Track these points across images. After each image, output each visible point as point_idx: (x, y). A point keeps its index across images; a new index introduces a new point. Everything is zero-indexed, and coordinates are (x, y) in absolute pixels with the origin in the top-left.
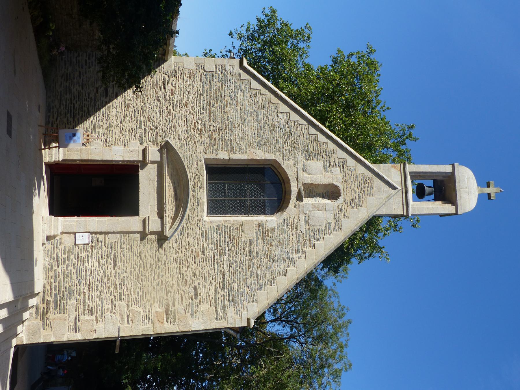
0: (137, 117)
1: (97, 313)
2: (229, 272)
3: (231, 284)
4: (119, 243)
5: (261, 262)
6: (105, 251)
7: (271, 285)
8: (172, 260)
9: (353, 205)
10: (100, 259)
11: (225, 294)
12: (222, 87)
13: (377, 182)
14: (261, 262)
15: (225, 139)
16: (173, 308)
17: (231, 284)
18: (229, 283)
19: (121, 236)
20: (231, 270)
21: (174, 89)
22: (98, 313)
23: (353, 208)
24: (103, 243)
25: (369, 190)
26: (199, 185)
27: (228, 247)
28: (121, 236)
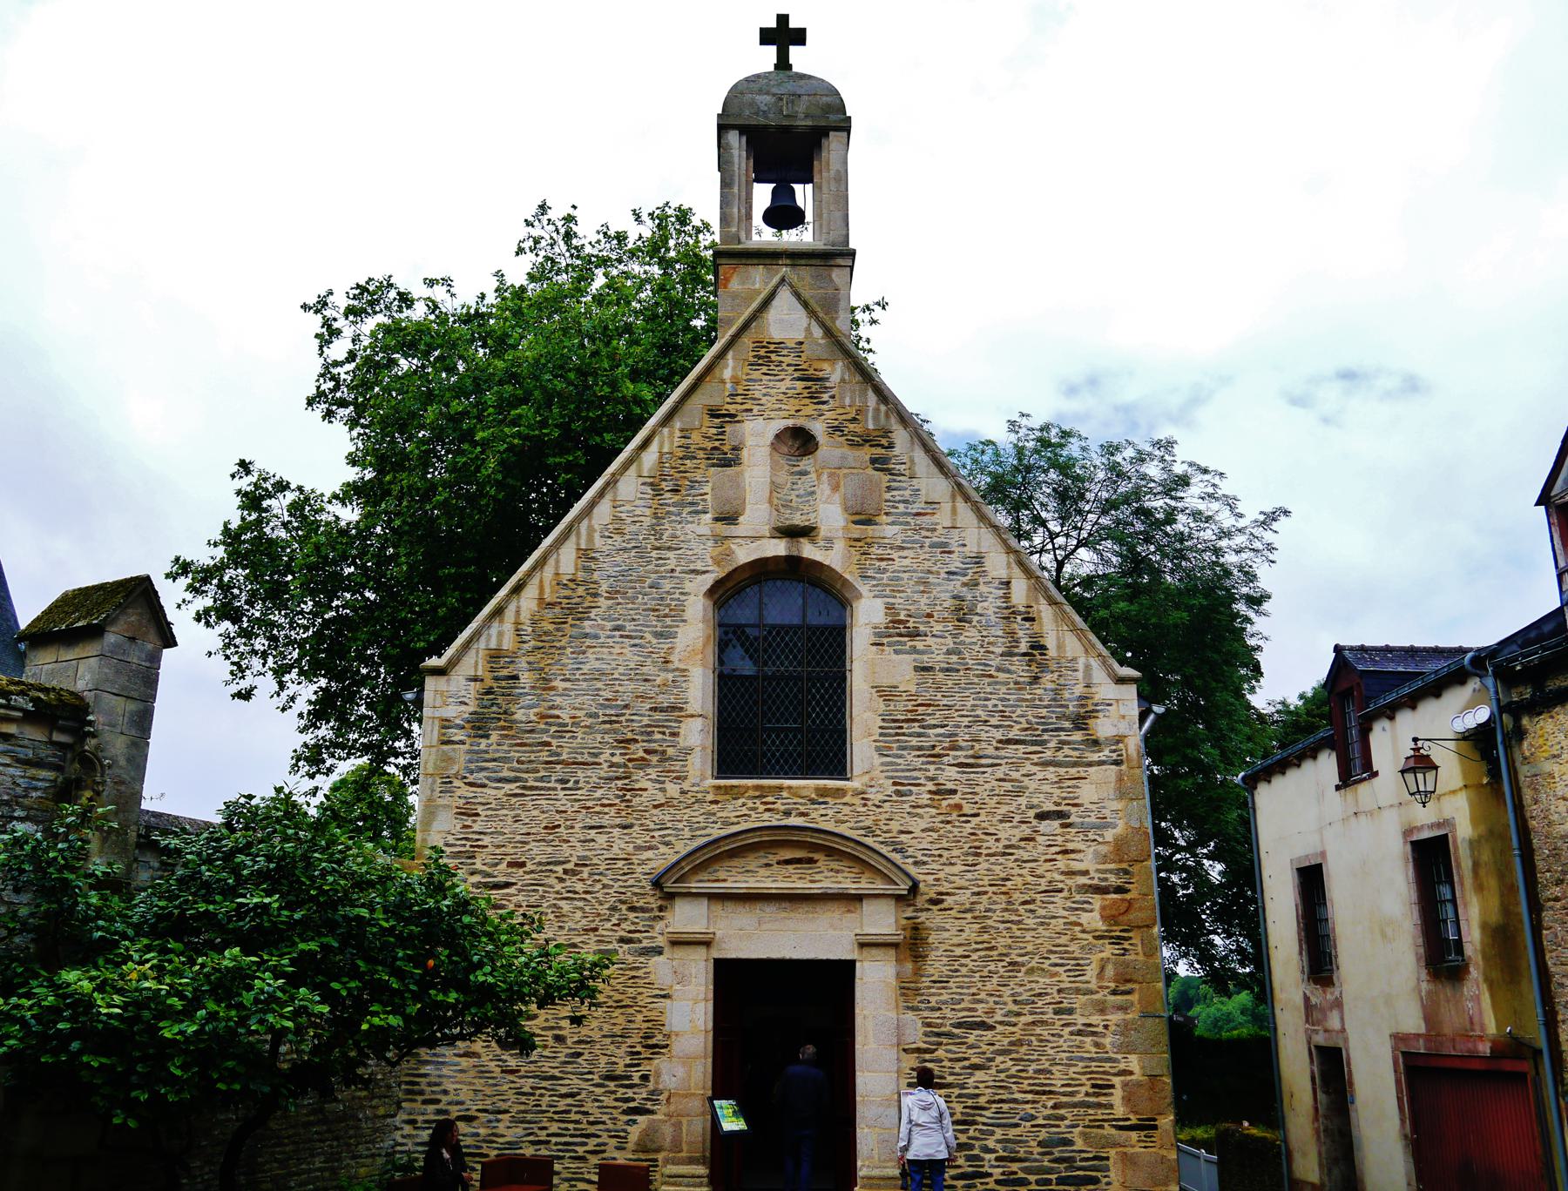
3: (1028, 722)
4: (926, 1014)
17: (1028, 722)
20: (994, 721)
21: (508, 859)
27: (935, 726)
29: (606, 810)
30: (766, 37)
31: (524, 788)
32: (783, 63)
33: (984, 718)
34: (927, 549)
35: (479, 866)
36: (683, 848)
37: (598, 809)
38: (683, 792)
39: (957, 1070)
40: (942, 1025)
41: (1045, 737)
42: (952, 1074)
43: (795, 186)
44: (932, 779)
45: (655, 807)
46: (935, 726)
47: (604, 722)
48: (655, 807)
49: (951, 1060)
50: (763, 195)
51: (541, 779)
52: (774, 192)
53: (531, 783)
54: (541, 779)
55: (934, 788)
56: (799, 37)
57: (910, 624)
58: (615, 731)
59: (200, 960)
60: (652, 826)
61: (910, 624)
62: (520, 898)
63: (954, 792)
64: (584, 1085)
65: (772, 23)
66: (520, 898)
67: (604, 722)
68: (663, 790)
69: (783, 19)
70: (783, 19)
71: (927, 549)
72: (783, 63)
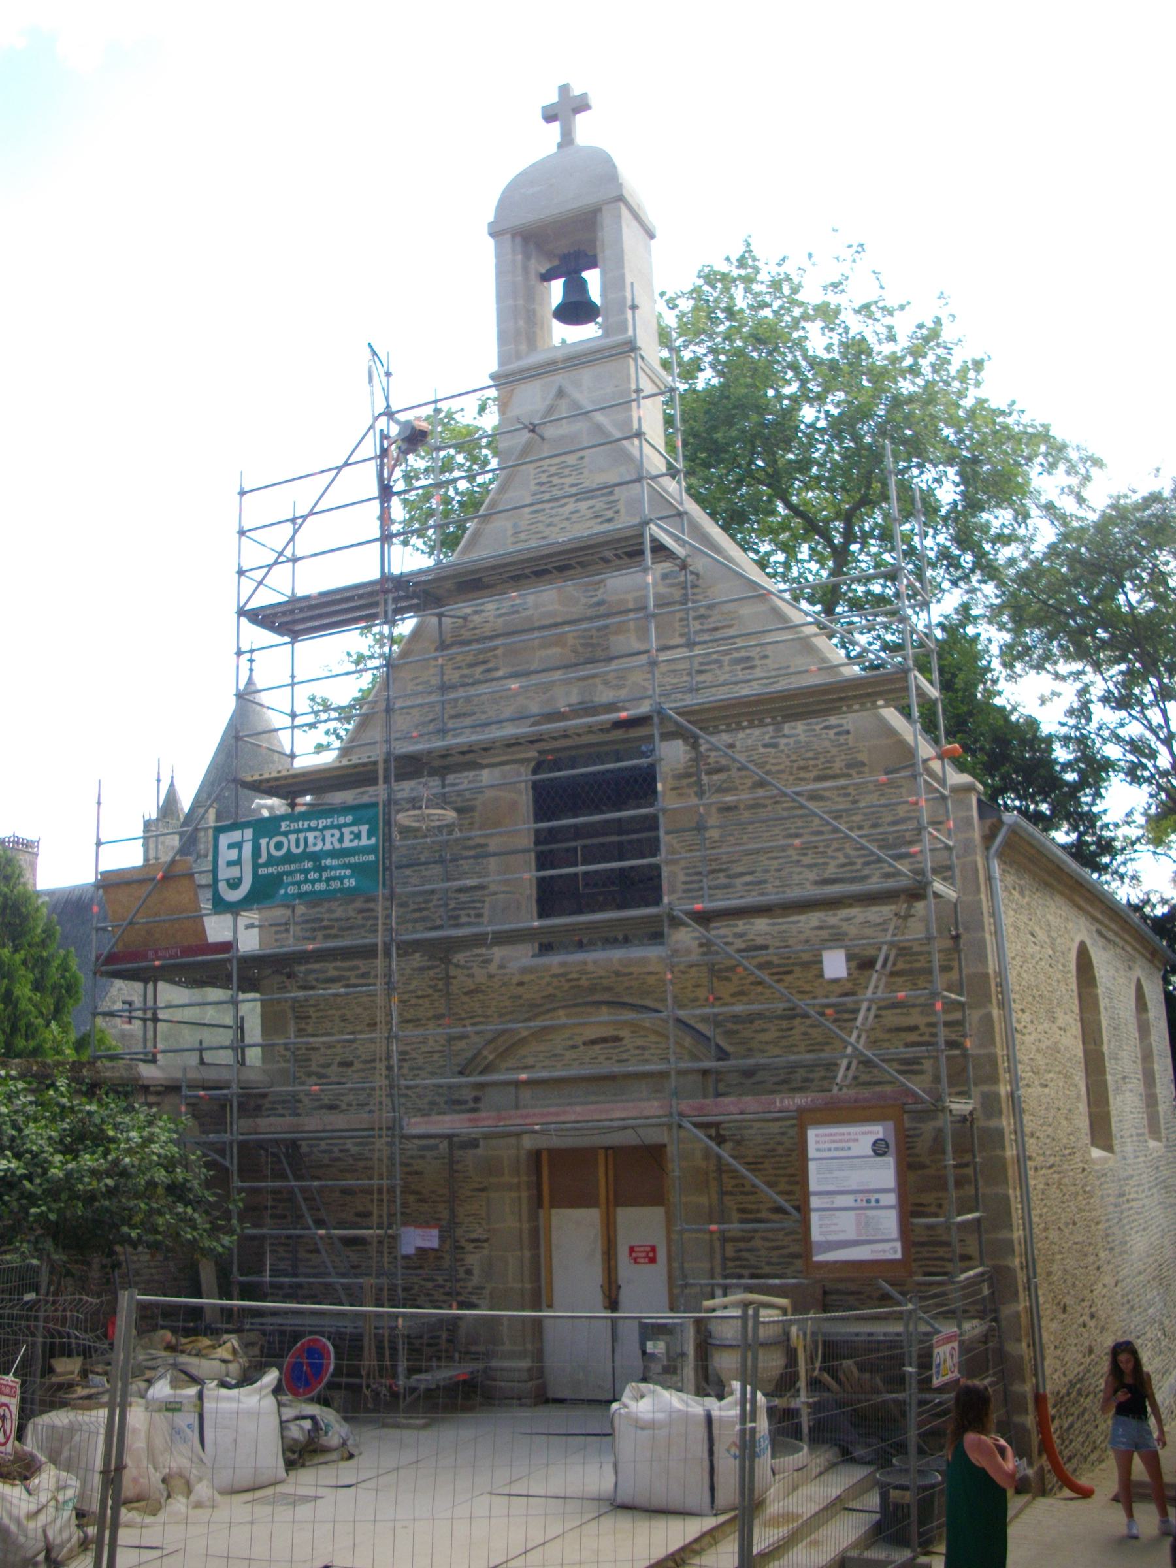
0: (412, 1157)
1: (942, 1259)
2: (815, 865)
3: (847, 856)
4: (740, 1198)
5: (782, 771)
6: (765, 1239)
7: (848, 732)
8: (784, 1043)
9: (610, 514)
10: (785, 1252)
11: (877, 873)
12: (326, 928)
13: (618, 1372)
14: (782, 771)
15: (455, 909)
16: (923, 1029)
17: (847, 856)
18: (843, 865)
19: (528, 851)
20: (807, 860)
21: (338, 1059)
22: (941, 1254)
23: (617, 512)
24: (742, 1245)
25: (567, 472)
26: (574, 976)
27: (742, 874)
28: (528, 851)
29: (421, 1001)
30: (550, 116)
31: (347, 986)
32: (567, 138)
33: (796, 858)
34: (727, 668)
35: (314, 1068)
36: (1083, 1107)
37: (413, 1001)
38: (491, 976)
39: (774, 1260)
40: (758, 1211)
41: (866, 872)
42: (769, 1263)
43: (585, 275)
44: (741, 935)
45: (466, 994)
46: (742, 874)
47: (414, 911)
48: (466, 994)
49: (769, 1249)
50: (556, 290)
51: (363, 975)
52: (566, 285)
53: (353, 981)
54: (363, 975)
55: (743, 946)
56: (582, 105)
57: (711, 760)
58: (424, 919)
59: (494, 463)
60: (463, 1015)
61: (711, 760)
62: (351, 1097)
63: (766, 947)
64: (415, 1279)
65: (554, 98)
66: (351, 1097)
67: (414, 911)
68: (471, 976)
69: (564, 89)
70: (564, 89)
71: (727, 668)
72: (567, 138)
